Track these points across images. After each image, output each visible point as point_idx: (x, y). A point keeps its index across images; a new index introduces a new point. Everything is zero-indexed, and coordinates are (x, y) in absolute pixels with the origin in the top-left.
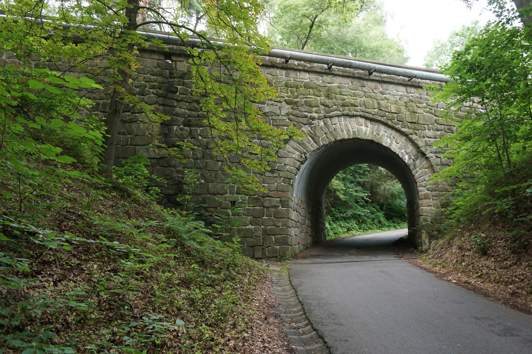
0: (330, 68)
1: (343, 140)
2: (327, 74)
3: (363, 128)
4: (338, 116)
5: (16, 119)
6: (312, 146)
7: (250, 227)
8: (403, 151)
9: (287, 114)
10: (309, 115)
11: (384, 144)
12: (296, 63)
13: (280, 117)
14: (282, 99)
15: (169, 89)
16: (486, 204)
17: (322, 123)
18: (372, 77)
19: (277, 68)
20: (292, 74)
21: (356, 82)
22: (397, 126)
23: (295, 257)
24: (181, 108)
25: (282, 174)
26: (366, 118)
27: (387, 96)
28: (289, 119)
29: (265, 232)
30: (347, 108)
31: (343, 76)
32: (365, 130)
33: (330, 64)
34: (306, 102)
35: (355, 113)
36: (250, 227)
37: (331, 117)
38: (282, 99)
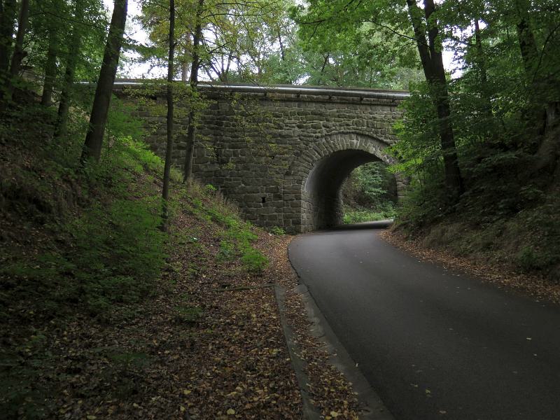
0: (330, 98)
1: (340, 151)
2: (329, 103)
3: (355, 141)
4: (336, 134)
5: (220, 243)
6: (316, 156)
7: (275, 214)
8: (385, 156)
9: (299, 136)
10: (314, 135)
11: (371, 153)
12: (315, 97)
13: (294, 138)
14: (294, 125)
15: (217, 123)
16: (286, 156)
17: (324, 140)
18: (362, 102)
19: (291, 101)
20: (303, 105)
21: (351, 106)
22: (380, 138)
23: (306, 231)
24: (226, 136)
25: (296, 177)
26: (358, 134)
27: (375, 115)
28: (300, 139)
29: (286, 217)
30: (342, 127)
31: (340, 103)
32: (356, 143)
33: (361, 97)
34: (312, 125)
35: (348, 131)
36: (275, 214)
37: (330, 135)
38: (294, 125)
